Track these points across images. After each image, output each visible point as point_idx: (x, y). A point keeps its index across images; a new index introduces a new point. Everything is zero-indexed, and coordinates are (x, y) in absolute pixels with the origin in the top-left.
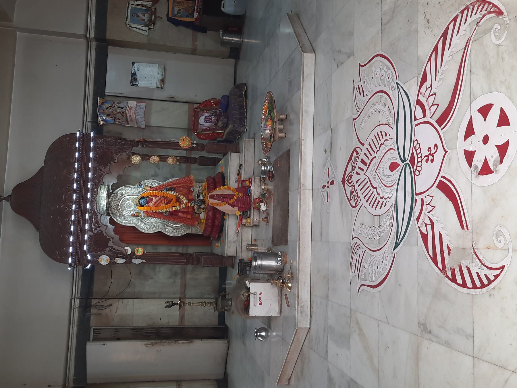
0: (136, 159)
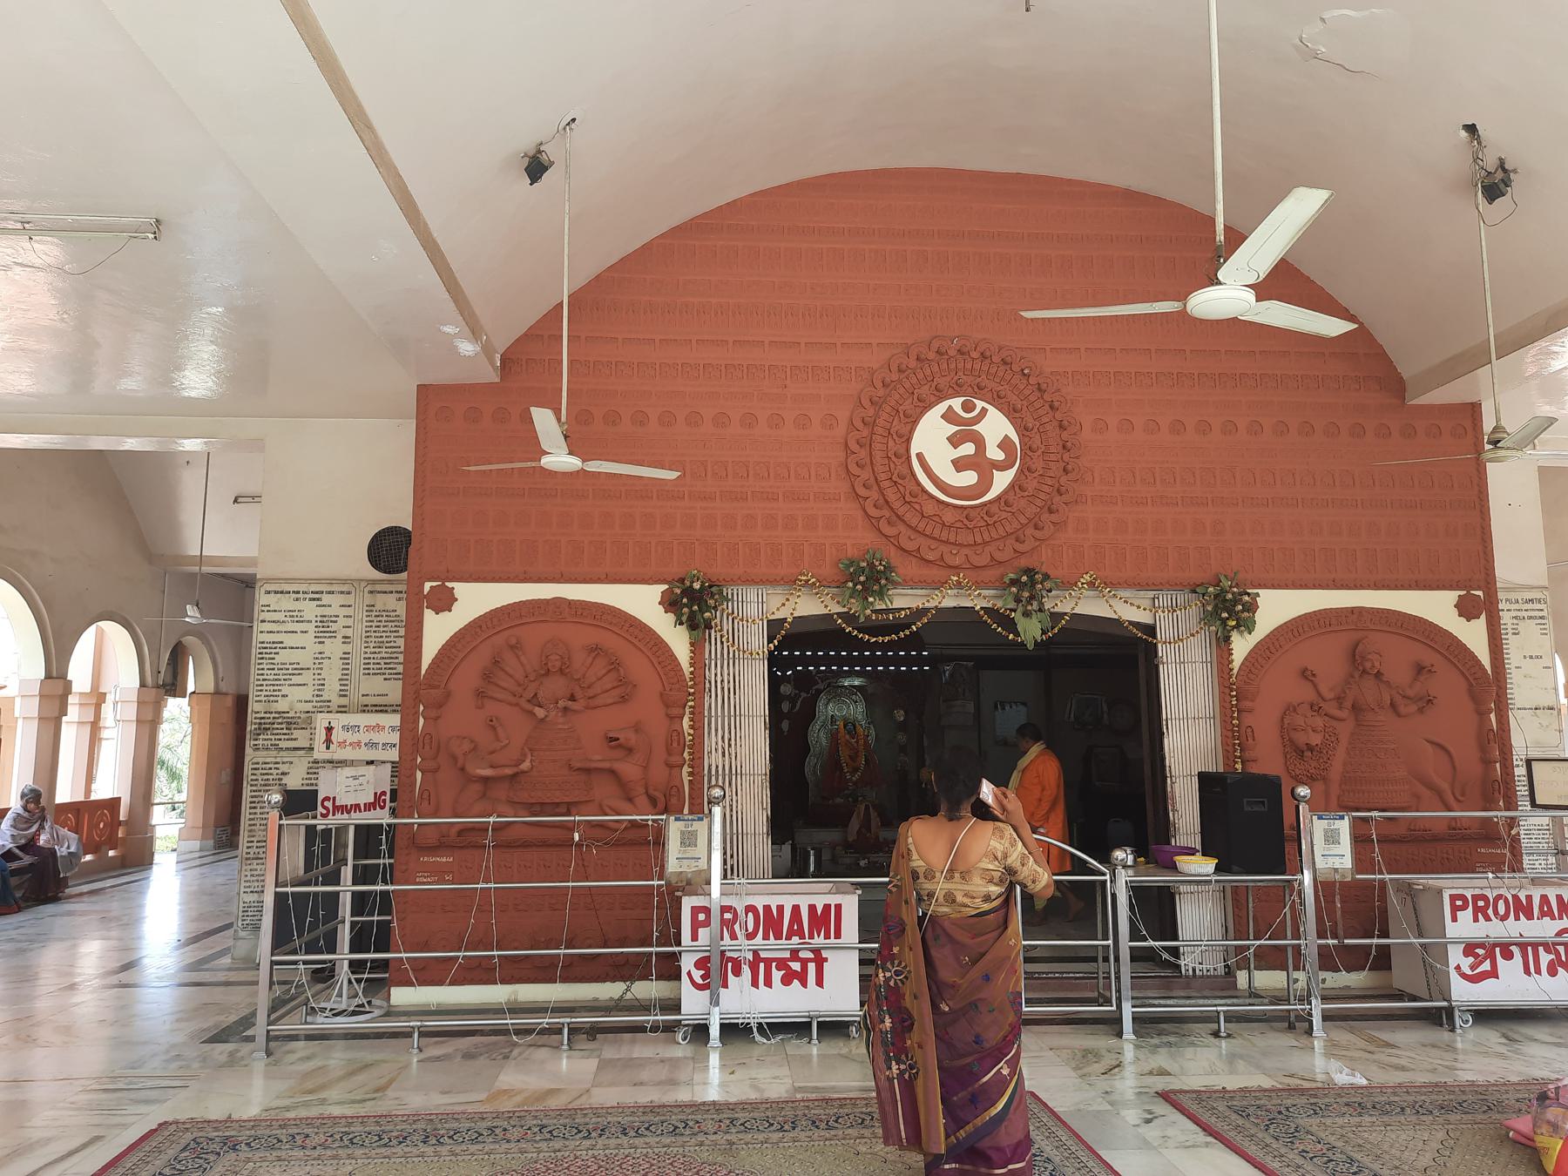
0: (900, 715)
